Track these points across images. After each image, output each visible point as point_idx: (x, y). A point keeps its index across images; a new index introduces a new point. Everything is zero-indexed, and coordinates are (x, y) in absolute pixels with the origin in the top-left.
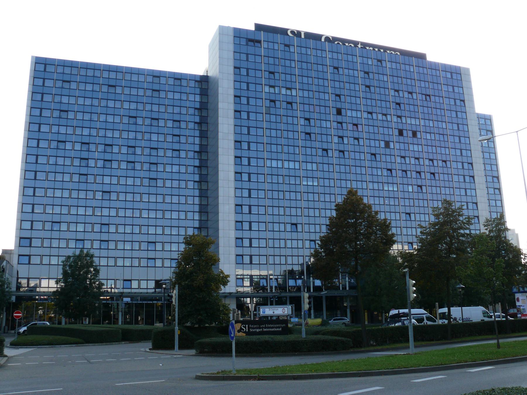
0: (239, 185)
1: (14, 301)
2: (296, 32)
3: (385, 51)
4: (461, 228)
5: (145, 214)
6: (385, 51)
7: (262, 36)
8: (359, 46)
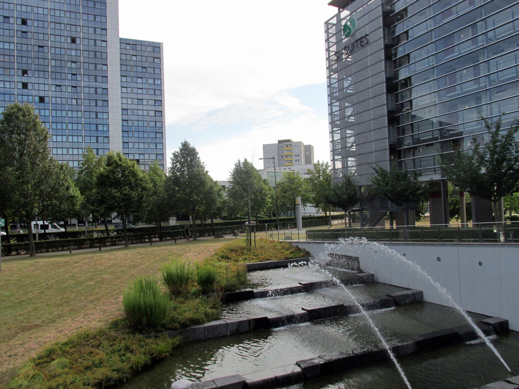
4: (133, 198)
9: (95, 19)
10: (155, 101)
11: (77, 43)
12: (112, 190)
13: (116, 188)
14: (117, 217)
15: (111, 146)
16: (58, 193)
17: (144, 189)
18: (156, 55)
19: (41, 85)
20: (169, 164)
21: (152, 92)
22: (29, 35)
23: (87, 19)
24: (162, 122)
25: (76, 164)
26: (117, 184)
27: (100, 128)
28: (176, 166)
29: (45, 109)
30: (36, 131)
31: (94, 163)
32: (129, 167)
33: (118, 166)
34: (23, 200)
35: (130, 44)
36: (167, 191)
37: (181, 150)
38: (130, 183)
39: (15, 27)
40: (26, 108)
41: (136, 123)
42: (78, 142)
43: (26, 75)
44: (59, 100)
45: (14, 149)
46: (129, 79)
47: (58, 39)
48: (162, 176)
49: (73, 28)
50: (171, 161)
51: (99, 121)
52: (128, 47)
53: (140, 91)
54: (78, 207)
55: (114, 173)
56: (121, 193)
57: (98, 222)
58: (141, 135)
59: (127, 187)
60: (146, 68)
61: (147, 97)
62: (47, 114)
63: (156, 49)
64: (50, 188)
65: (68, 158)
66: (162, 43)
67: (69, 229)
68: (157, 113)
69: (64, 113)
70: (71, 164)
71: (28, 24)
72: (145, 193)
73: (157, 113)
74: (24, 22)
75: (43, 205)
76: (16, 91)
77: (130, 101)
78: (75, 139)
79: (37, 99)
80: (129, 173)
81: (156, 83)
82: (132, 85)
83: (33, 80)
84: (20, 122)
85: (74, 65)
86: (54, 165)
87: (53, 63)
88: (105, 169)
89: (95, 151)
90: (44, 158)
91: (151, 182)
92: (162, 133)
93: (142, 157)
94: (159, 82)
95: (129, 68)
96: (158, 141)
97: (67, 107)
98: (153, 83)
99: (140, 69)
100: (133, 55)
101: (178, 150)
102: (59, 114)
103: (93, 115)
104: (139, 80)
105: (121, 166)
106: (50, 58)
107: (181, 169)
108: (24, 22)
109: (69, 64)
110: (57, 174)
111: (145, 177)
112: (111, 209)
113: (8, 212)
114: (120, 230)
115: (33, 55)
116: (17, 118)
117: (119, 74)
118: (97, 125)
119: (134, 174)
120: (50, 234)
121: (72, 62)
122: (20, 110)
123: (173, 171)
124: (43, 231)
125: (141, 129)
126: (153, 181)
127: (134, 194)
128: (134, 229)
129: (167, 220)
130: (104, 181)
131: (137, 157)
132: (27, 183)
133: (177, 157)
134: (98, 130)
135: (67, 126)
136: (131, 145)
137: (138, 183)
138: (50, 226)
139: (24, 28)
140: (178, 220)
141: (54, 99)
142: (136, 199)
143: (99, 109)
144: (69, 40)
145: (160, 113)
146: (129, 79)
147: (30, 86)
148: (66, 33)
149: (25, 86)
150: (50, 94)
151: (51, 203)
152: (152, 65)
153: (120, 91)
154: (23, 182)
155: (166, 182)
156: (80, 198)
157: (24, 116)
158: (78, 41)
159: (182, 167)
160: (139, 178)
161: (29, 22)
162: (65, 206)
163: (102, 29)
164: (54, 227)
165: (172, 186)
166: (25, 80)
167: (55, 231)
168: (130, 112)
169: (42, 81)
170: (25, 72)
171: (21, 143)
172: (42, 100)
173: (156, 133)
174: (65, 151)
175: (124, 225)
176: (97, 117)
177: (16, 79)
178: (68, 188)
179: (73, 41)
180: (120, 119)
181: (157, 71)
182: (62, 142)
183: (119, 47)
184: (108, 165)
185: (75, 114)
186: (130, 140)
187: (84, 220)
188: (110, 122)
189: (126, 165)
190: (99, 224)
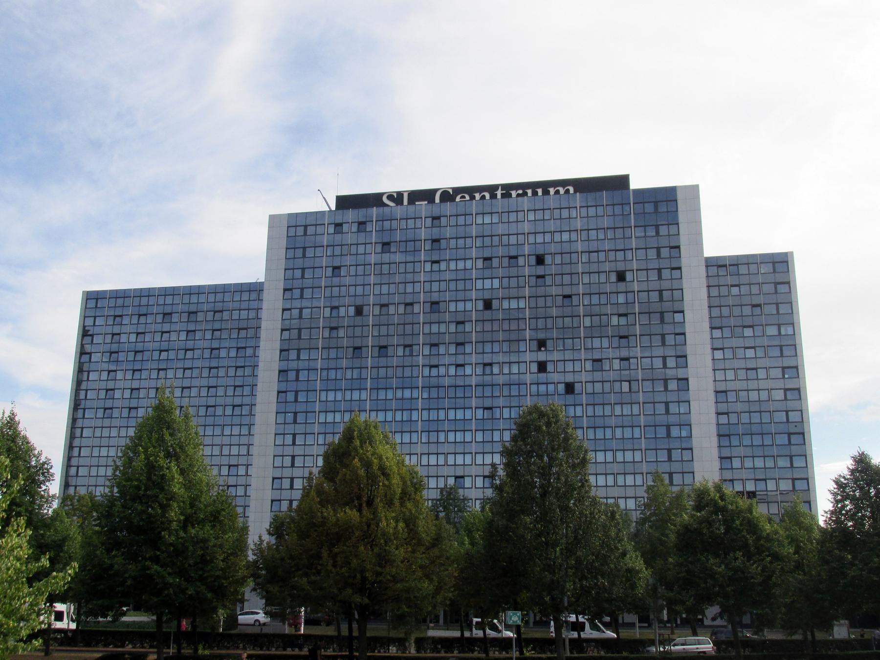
0: (279, 450)
1: (154, 618)
2: (451, 191)
3: (546, 193)
4: (752, 578)
5: (620, 480)
6: (546, 193)
7: (351, 215)
8: (499, 193)
9: (657, 233)
10: (784, 368)
11: (628, 280)
12: (708, 560)
13: (717, 556)
14: (721, 615)
15: (697, 466)
16: (608, 565)
17: (776, 557)
18: (780, 278)
19: (570, 364)
20: (824, 505)
21: (776, 352)
22: (548, 280)
23: (643, 234)
24: (802, 412)
25: (631, 504)
26: (720, 546)
27: (675, 432)
28: (844, 507)
29: (575, 405)
30: (568, 451)
31: (667, 504)
32: (741, 511)
33: (717, 509)
34: (548, 577)
35: (725, 266)
36: (827, 562)
37: (852, 472)
38: (745, 546)
39: (527, 271)
40: (552, 410)
41: (745, 418)
42: (634, 462)
43: (543, 349)
44: (598, 387)
45: (533, 485)
46: (727, 332)
47: (595, 278)
48: (812, 529)
49: (620, 255)
50: (830, 497)
51: (672, 419)
52: (722, 272)
53: (750, 353)
54: (640, 591)
55: (710, 523)
56: (727, 565)
57: (676, 622)
58: (757, 440)
59: (739, 554)
60: (759, 305)
61: (766, 362)
62: (579, 414)
63: (779, 266)
64: (593, 555)
65: (615, 492)
66: (792, 253)
67: (625, 634)
68: (788, 393)
69: (608, 408)
70: (622, 503)
71: (546, 263)
72: (777, 566)
73: (788, 393)
74: (540, 260)
75: (582, 587)
76: (528, 378)
77: (730, 375)
78: (629, 456)
79: (561, 388)
80: (741, 525)
81: (783, 333)
82: (735, 342)
83: (556, 356)
84: (543, 436)
85: (623, 321)
86: (599, 512)
87: (587, 322)
88: (692, 516)
89: (666, 477)
90: (580, 500)
91: (790, 543)
92: (803, 434)
93: (761, 486)
94: (790, 332)
95: (725, 311)
96: (795, 450)
97: (612, 398)
98: (776, 333)
99: (747, 310)
100: (732, 286)
101: (846, 473)
102: (599, 411)
103: (661, 409)
104: (748, 332)
105: (723, 510)
106: (582, 314)
107: (855, 514)
108: (540, 260)
109: (615, 320)
110: (604, 527)
111: (776, 533)
112: (708, 598)
113: (524, 596)
114: (723, 642)
115: (554, 312)
116: (538, 429)
117: (706, 325)
118: (668, 427)
119: (752, 526)
120: (589, 641)
121: (620, 315)
122: (542, 415)
123: (838, 518)
124: (575, 635)
125: (755, 429)
126: (793, 540)
127: (754, 568)
128: (754, 641)
129: (829, 628)
130: (692, 541)
131: (750, 487)
132: (556, 544)
133: (844, 488)
134: (672, 436)
135: (613, 433)
136: (736, 463)
137: (762, 545)
138: (587, 625)
139: (540, 270)
140: (852, 625)
141: (589, 386)
142: (759, 579)
143: (672, 397)
144: (613, 277)
145: (797, 393)
146: (727, 332)
147: (550, 367)
148: (607, 267)
149: (542, 367)
150: (584, 377)
151: (596, 584)
152: (773, 299)
153: (710, 358)
154: (547, 543)
155: (822, 543)
156: (645, 575)
157: (548, 424)
158: (629, 276)
159: (858, 508)
160: (764, 534)
161: (548, 259)
162: (618, 591)
163: (672, 248)
164: (594, 627)
165: (837, 552)
166: (542, 356)
167: (595, 635)
168: (732, 397)
169: (568, 355)
170: (542, 344)
171: (545, 473)
172: (570, 388)
173: (789, 434)
174: (610, 479)
175: (735, 633)
176: (667, 412)
177: (528, 357)
178: (624, 554)
179: (621, 277)
180: (713, 410)
181: (783, 309)
182: (635, 486)
183: (705, 275)
184: (698, 507)
185: (627, 410)
186: (736, 452)
187: (652, 616)
188: (694, 418)
189: (734, 507)
190: (677, 626)
